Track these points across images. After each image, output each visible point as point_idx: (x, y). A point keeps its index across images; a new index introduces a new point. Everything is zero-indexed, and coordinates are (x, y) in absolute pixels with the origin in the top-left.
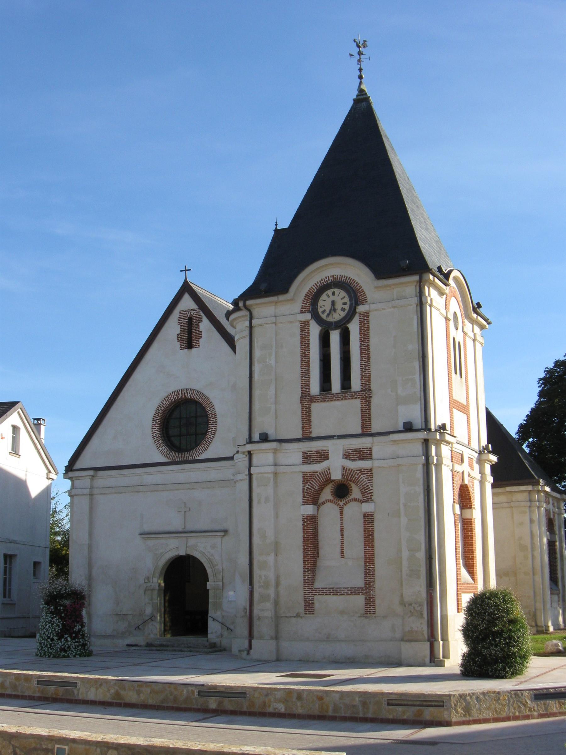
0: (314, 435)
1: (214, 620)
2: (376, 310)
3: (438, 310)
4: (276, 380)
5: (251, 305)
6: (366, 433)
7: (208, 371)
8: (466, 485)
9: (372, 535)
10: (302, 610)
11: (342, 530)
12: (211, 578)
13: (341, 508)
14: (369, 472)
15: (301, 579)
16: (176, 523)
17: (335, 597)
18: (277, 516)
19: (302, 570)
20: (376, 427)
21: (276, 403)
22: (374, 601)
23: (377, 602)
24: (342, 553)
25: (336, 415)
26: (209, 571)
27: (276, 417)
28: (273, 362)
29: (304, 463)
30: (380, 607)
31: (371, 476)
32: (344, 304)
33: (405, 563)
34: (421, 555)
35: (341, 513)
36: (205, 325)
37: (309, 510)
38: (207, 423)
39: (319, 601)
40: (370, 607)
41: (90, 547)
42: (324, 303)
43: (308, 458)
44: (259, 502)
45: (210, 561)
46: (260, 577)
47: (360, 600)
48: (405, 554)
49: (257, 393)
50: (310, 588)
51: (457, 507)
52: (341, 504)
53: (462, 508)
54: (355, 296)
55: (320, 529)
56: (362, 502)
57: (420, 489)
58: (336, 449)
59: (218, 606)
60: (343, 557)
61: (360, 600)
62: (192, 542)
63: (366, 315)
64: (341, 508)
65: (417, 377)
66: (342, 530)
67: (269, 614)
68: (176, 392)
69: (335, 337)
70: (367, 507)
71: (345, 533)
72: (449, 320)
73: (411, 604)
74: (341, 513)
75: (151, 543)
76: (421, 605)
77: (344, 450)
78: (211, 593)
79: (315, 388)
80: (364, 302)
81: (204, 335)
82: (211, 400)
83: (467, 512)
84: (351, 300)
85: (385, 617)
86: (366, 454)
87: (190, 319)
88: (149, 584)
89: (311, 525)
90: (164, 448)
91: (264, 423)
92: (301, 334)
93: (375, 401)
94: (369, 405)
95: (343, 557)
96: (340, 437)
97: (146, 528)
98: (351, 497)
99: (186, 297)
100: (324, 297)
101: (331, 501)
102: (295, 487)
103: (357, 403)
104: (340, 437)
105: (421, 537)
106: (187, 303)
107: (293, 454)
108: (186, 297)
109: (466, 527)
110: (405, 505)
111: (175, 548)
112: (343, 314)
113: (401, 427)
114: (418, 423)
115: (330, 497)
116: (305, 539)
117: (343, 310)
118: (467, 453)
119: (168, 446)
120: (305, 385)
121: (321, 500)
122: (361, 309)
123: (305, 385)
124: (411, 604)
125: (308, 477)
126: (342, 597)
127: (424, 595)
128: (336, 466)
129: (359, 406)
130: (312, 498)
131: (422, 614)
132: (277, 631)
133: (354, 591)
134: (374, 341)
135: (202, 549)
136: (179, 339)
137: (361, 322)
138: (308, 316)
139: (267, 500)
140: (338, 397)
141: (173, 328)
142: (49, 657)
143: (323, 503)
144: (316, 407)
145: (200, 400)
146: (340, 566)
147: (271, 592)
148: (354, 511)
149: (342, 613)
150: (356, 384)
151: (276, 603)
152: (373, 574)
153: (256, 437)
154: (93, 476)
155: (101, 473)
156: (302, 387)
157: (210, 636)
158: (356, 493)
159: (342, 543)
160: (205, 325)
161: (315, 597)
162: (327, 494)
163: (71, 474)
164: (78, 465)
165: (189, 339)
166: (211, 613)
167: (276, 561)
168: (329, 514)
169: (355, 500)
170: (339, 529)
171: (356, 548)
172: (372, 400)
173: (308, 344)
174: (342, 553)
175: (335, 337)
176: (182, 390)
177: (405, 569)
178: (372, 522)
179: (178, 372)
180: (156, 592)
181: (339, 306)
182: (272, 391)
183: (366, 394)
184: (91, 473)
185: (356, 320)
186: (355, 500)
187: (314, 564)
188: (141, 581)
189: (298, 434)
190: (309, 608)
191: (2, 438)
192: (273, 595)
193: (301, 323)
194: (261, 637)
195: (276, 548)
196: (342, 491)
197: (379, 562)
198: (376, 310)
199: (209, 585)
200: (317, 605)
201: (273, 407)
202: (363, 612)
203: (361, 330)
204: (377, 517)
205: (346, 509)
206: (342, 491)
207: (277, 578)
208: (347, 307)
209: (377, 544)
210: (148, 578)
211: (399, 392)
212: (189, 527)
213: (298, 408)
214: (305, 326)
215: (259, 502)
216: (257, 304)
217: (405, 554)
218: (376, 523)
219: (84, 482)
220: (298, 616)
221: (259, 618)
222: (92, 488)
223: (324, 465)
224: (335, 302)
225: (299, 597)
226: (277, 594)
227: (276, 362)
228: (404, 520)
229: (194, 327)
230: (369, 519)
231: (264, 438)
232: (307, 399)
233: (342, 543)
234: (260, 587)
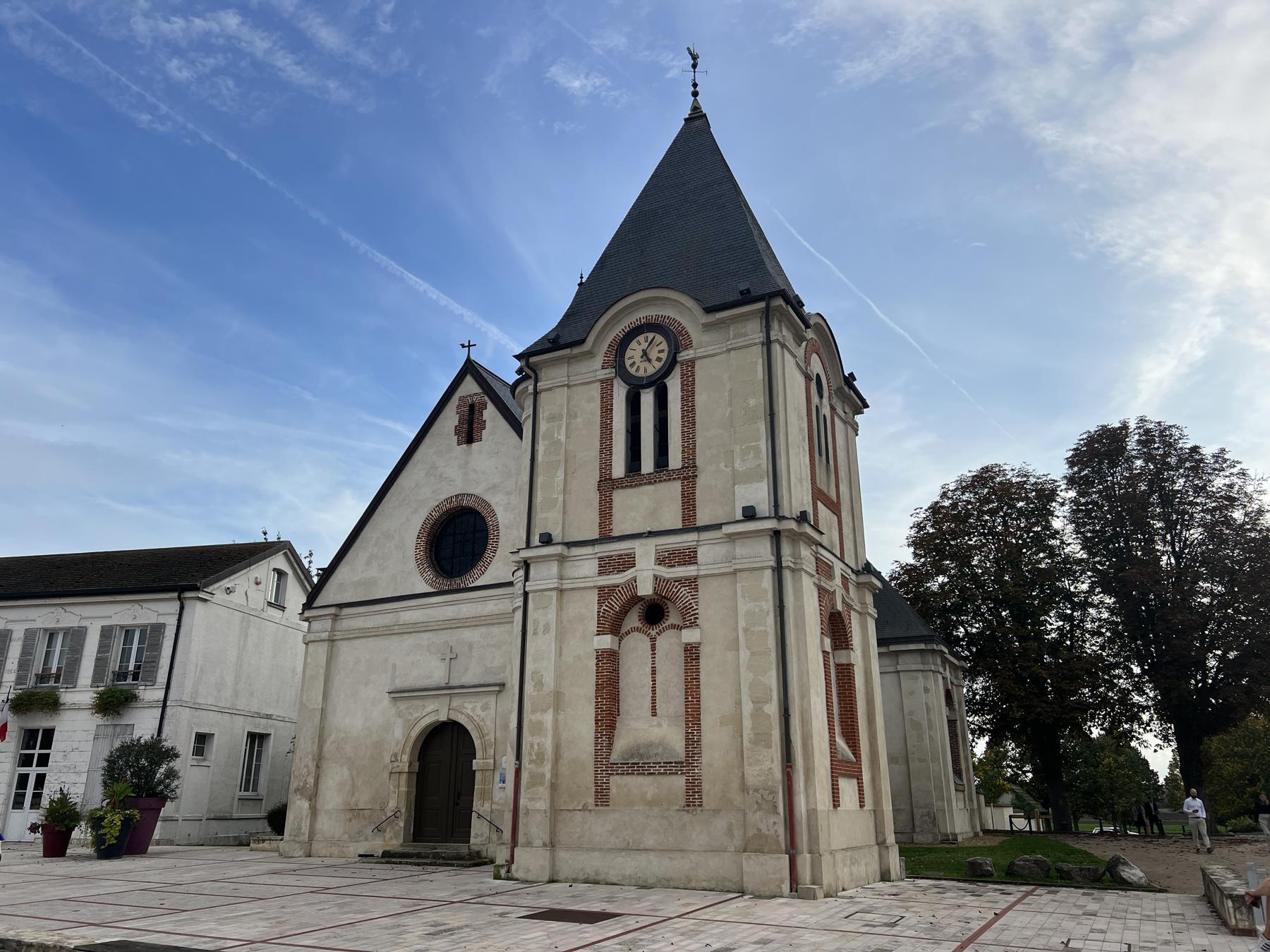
0: (615, 533)
1: (479, 816)
2: (704, 357)
3: (795, 357)
4: (566, 461)
5: (537, 364)
6: (689, 527)
7: (485, 471)
8: (839, 613)
9: (698, 679)
10: (591, 801)
11: (654, 672)
12: (479, 753)
13: (653, 640)
14: (692, 582)
15: (591, 749)
16: (435, 673)
17: (640, 779)
18: (560, 653)
19: (593, 735)
20: (703, 518)
21: (565, 491)
22: (700, 785)
23: (706, 786)
24: (654, 708)
25: (643, 507)
26: (477, 743)
27: (564, 513)
28: (563, 438)
29: (600, 574)
30: (709, 789)
31: (696, 589)
32: (660, 352)
33: (747, 723)
34: (773, 709)
35: (653, 648)
36: (490, 412)
37: (607, 641)
38: (487, 538)
39: (616, 782)
40: (694, 792)
41: (323, 711)
42: (634, 351)
43: (606, 565)
44: (535, 633)
45: (479, 729)
46: (532, 746)
47: (679, 782)
48: (748, 707)
49: (540, 480)
50: (611, 764)
51: (828, 641)
52: (653, 633)
53: (836, 647)
54: (676, 340)
55: (622, 672)
56: (680, 628)
57: (768, 605)
58: (646, 552)
59: (487, 795)
60: (654, 714)
61: (679, 782)
62: (456, 703)
63: (691, 363)
64: (653, 640)
65: (763, 445)
66: (654, 672)
67: (543, 805)
68: (449, 500)
69: (647, 400)
70: (690, 636)
71: (659, 678)
72: (811, 380)
73: (757, 790)
74: (653, 648)
75: (403, 706)
76: (773, 792)
77: (657, 552)
78: (478, 776)
79: (619, 470)
80: (689, 346)
81: (488, 425)
82: (494, 507)
83: (842, 657)
84: (669, 346)
85: (717, 812)
86: (689, 557)
87: (472, 407)
88: (396, 764)
89: (609, 664)
90: (430, 574)
91: (547, 521)
92: (602, 398)
93: (702, 481)
94: (694, 488)
95: (654, 714)
96: (651, 534)
97: (399, 684)
98: (667, 623)
99: (469, 378)
100: (634, 344)
101: (638, 630)
102: (587, 608)
103: (676, 487)
104: (651, 534)
105: (772, 679)
106: (470, 387)
107: (585, 567)
108: (469, 378)
109: (844, 676)
110: (746, 630)
111: (434, 712)
112: (658, 365)
113: (739, 516)
114: (764, 508)
115: (638, 624)
116: (599, 688)
117: (659, 359)
118: (838, 567)
119: (436, 571)
120: (606, 465)
121: (624, 630)
122: (684, 356)
123: (606, 465)
124: (757, 790)
125: (605, 593)
126: (651, 778)
127: (778, 774)
128: (645, 576)
129: (680, 489)
130: (613, 625)
131: (775, 807)
132: (553, 832)
133: (671, 768)
134: (700, 399)
135: (470, 712)
136: (457, 431)
137: (683, 375)
138: (609, 373)
139: (547, 629)
140: (651, 480)
141: (450, 418)
142: (56, 845)
143: (628, 633)
144: (619, 497)
145: (479, 508)
146: (649, 727)
147: (547, 769)
148: (670, 642)
149: (650, 804)
150: (675, 460)
151: (554, 787)
152: (699, 741)
153: (536, 540)
154: (336, 615)
155: (346, 611)
156: (601, 469)
157: (472, 840)
158: (673, 618)
159: (654, 692)
160: (490, 412)
161: (612, 778)
162: (633, 620)
163: (307, 614)
164: (318, 602)
165: (469, 432)
166: (476, 805)
167: (556, 721)
168: (636, 647)
169: (673, 627)
170: (649, 670)
171: (673, 701)
172: (697, 480)
173: (611, 410)
174: (654, 708)
175: (647, 400)
176: (457, 496)
177: (747, 733)
178: (698, 658)
179: (454, 473)
180: (405, 776)
181: (653, 354)
182: (560, 475)
183: (689, 474)
184: (332, 610)
185: (677, 371)
186: (673, 627)
187: (612, 727)
188: (387, 759)
189: (595, 535)
190: (602, 796)
191: (257, 584)
192: (548, 776)
193: (602, 381)
194: (529, 844)
195: (557, 702)
196: (654, 612)
197: (709, 721)
198: (704, 357)
199: (476, 764)
200: (613, 790)
201: (561, 498)
202: (682, 802)
203: (683, 385)
204: (704, 651)
205: (660, 642)
206: (654, 612)
207: (557, 747)
208: (664, 356)
209: (705, 692)
210: (396, 755)
211: (737, 465)
212: (454, 682)
213: (595, 497)
214: (606, 385)
215: (535, 633)
216: (545, 362)
217: (748, 707)
218: (702, 661)
219: (322, 627)
220: (585, 809)
221: (527, 812)
222: (333, 629)
223: (629, 574)
224: (645, 357)
225: (587, 778)
226: (555, 774)
227: (568, 437)
228: (744, 654)
229: (476, 416)
230: (692, 653)
231: (547, 540)
232: (607, 485)
233: (654, 692)
234: (531, 762)
